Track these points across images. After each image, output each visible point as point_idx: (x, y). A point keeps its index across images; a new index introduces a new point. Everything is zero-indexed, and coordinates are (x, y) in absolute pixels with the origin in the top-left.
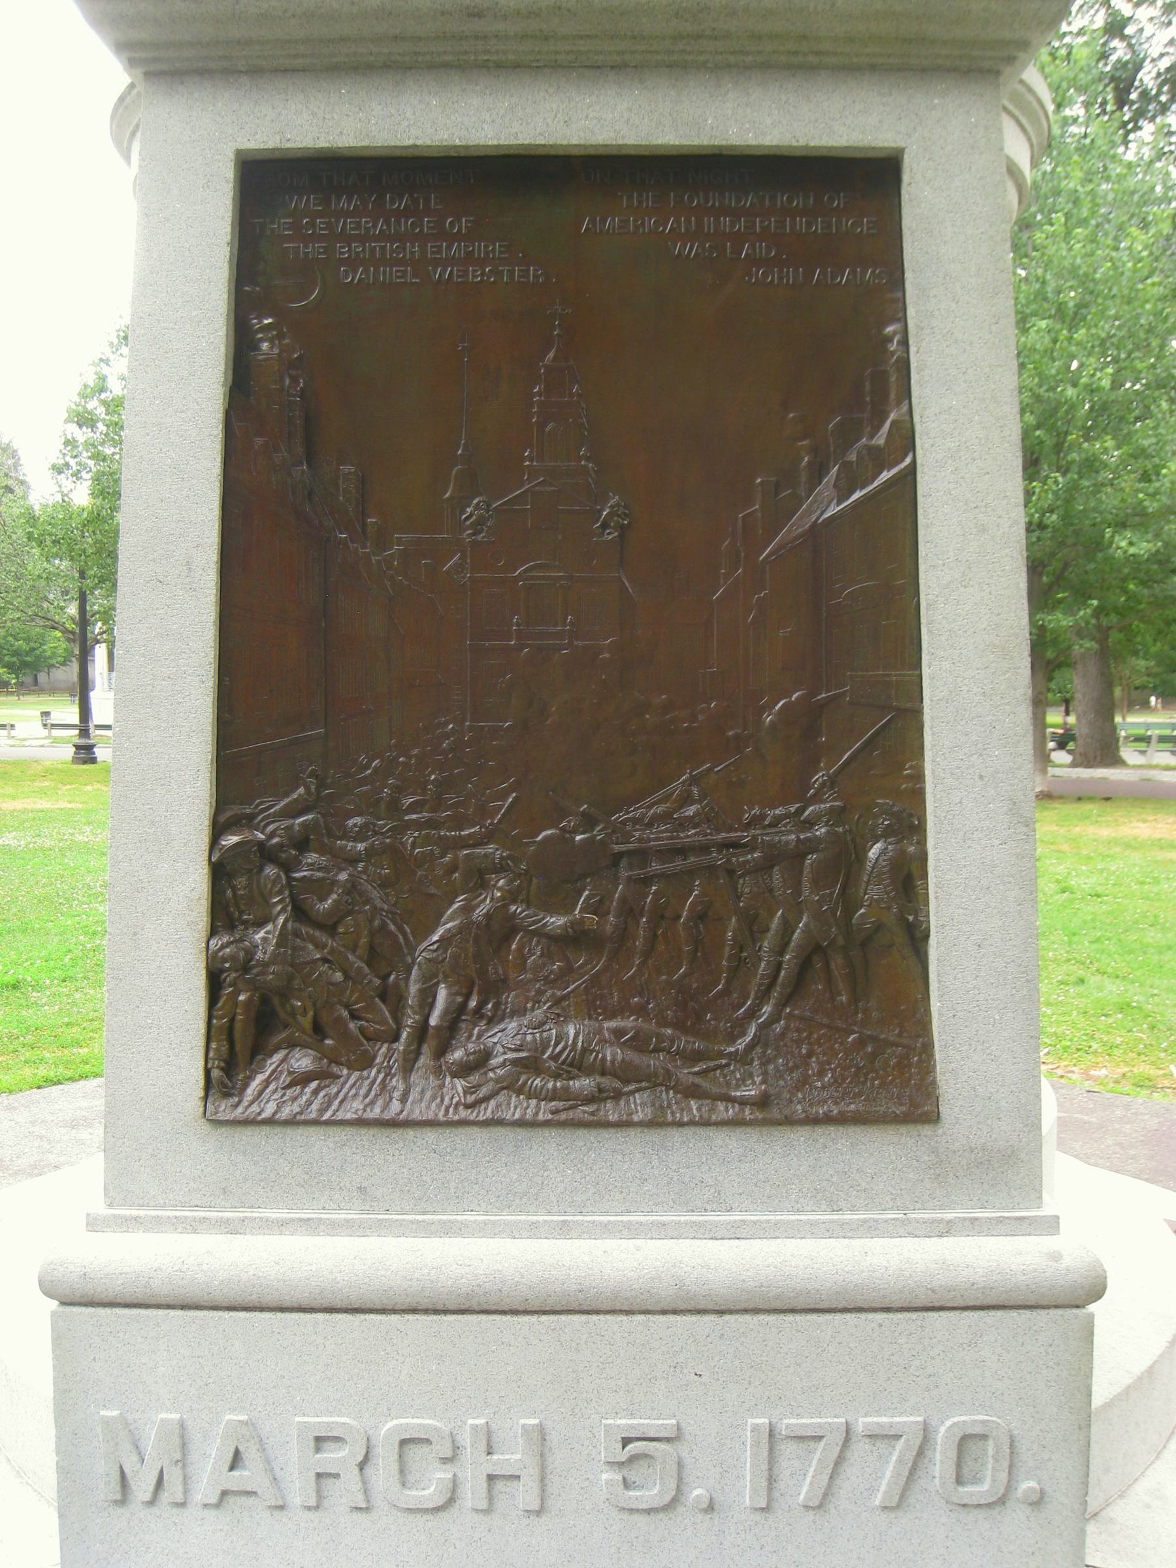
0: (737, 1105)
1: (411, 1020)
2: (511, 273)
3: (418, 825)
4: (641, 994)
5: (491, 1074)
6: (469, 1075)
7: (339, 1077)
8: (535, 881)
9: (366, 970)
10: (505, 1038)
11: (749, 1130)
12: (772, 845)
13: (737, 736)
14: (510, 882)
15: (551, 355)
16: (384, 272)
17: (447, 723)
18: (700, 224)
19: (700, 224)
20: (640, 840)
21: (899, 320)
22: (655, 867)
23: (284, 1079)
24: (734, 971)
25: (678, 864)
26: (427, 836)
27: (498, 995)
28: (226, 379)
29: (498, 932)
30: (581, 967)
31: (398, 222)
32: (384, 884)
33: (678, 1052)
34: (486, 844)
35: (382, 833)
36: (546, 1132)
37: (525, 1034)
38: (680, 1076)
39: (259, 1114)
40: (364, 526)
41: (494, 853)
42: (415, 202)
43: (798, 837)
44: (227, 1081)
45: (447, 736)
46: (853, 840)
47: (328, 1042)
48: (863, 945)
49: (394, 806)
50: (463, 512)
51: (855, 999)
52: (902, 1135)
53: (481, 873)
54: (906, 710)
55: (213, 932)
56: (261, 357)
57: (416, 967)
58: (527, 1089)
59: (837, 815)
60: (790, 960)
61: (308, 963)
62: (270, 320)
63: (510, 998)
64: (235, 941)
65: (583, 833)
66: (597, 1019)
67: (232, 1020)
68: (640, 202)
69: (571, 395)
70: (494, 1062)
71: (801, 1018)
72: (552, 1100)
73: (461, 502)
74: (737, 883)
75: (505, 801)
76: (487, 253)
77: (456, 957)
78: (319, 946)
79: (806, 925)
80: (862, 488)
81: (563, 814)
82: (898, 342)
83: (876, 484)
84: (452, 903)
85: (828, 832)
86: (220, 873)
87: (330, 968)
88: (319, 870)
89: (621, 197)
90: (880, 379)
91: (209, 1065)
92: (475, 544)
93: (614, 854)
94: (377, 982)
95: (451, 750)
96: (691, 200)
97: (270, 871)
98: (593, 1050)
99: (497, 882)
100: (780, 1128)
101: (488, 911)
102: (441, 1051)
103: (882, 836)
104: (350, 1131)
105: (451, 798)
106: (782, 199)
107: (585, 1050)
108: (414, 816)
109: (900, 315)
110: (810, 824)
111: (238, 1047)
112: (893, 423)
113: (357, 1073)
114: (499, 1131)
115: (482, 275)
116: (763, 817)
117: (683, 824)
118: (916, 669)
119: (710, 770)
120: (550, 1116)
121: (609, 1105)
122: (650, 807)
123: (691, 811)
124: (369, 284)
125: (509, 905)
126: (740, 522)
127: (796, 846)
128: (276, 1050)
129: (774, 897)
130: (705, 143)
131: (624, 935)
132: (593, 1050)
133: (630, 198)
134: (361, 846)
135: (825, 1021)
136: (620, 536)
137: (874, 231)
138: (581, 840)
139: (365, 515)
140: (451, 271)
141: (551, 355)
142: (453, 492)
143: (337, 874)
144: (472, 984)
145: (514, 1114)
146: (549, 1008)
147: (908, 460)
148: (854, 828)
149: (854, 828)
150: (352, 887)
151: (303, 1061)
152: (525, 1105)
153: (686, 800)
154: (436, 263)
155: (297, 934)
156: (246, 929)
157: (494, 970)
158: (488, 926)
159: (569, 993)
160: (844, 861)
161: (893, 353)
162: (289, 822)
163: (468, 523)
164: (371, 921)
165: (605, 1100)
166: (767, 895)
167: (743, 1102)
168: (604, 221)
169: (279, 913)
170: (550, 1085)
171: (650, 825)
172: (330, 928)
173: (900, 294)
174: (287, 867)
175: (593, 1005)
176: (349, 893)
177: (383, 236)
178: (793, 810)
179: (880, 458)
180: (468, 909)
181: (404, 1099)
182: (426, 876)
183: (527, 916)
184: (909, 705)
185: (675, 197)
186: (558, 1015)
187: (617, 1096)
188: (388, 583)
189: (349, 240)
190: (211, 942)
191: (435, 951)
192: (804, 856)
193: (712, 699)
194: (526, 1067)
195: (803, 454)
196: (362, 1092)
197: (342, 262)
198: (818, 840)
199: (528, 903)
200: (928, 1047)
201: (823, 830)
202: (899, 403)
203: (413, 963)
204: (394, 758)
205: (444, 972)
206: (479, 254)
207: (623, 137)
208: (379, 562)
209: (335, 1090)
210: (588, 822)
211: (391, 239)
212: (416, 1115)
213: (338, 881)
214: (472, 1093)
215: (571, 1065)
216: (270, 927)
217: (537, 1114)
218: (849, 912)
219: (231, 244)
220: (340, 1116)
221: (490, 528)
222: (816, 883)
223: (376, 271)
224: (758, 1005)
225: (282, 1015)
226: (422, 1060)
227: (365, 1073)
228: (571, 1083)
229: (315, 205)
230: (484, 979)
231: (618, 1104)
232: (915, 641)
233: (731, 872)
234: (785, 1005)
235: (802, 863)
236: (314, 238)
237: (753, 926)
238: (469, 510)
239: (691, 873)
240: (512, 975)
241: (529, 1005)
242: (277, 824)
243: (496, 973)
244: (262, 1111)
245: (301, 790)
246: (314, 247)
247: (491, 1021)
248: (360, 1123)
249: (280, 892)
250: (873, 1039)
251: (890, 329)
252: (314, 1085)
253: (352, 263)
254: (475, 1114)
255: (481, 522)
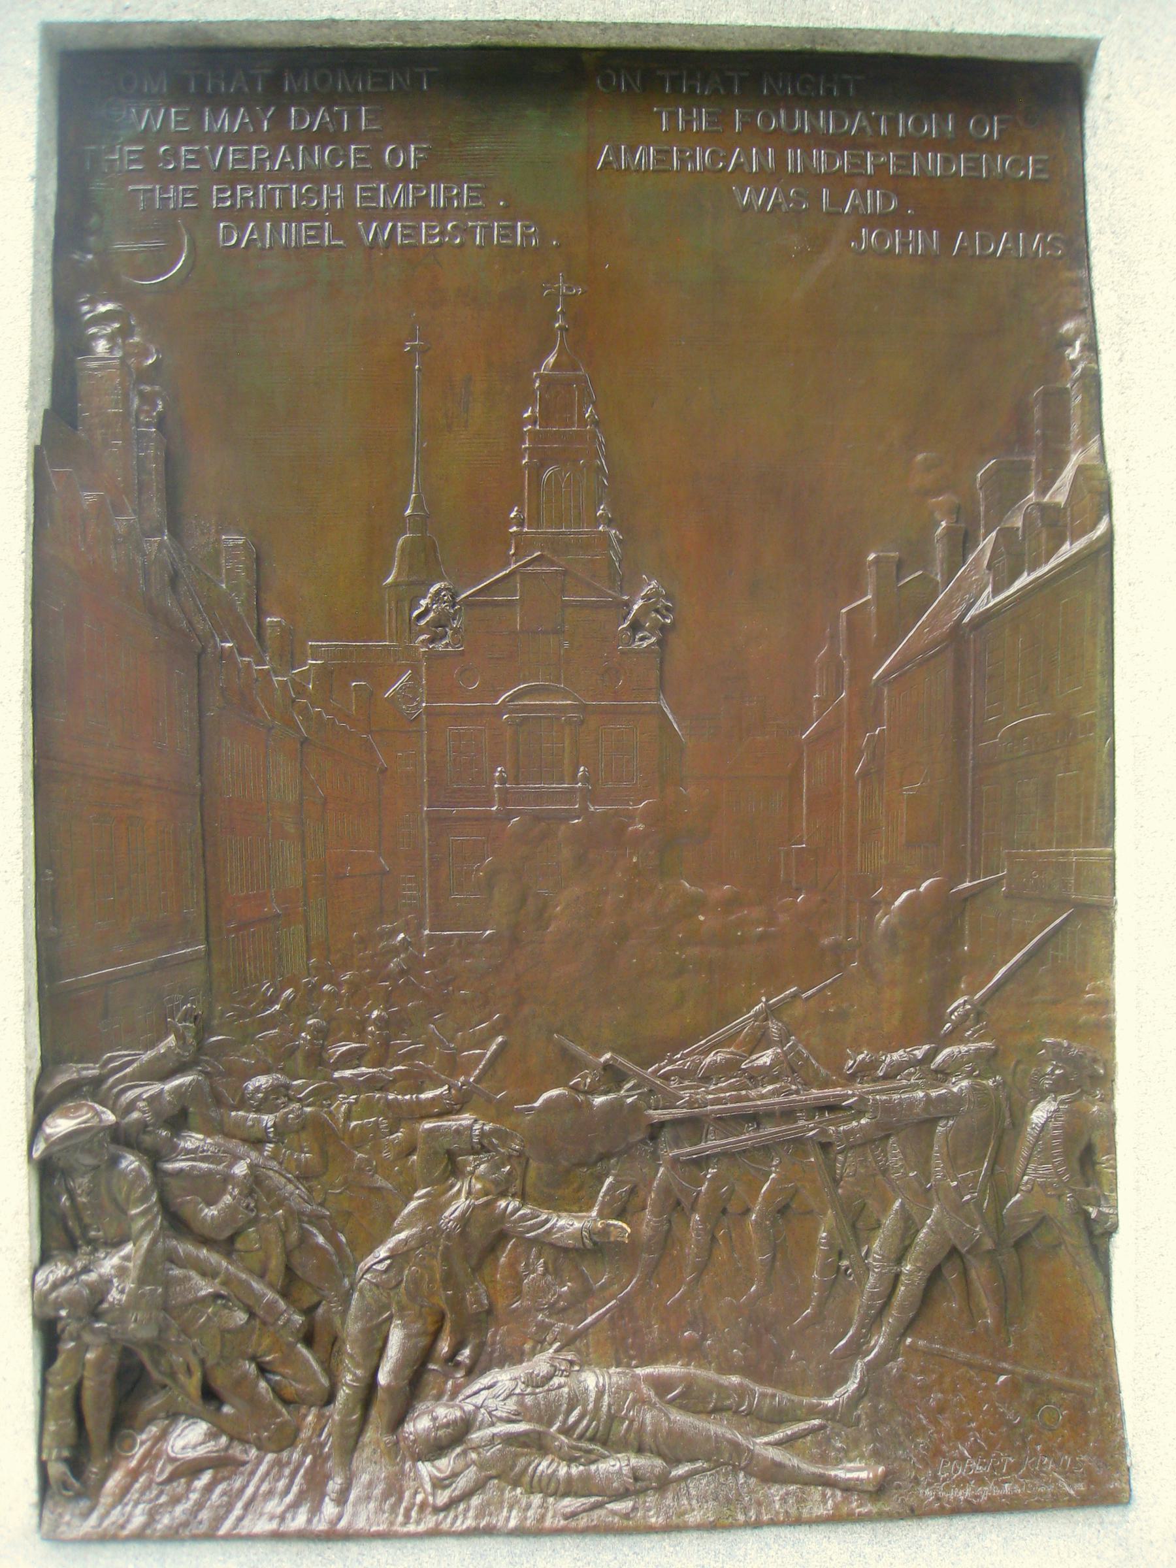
0: (839, 1493)
1: (350, 1378)
2: (488, 230)
3: (353, 1085)
4: (692, 1325)
5: (474, 1456)
6: (439, 1457)
7: (244, 1463)
8: (533, 1164)
9: (282, 1304)
10: (496, 1393)
11: (858, 1528)
12: (888, 1108)
13: (836, 948)
14: (496, 1167)
15: (551, 360)
16: (288, 231)
17: (394, 933)
18: (781, 160)
19: (781, 160)
20: (691, 1104)
21: (1083, 312)
22: (712, 1143)
23: (163, 1470)
24: (829, 1288)
25: (747, 1136)
26: (369, 1100)
27: (481, 1330)
28: (33, 398)
29: (485, 1240)
30: (603, 1287)
31: (309, 152)
32: (305, 1176)
33: (749, 1413)
34: (458, 1112)
35: (300, 1100)
36: (558, 1542)
37: (522, 1395)
38: (758, 1449)
39: (123, 1527)
40: (260, 627)
41: (470, 1127)
42: (337, 119)
43: (927, 1095)
44: (72, 1480)
45: (396, 951)
46: (1008, 1098)
47: (227, 1409)
48: (1018, 1245)
49: (317, 1059)
50: (414, 605)
51: (1005, 1319)
52: (1077, 1523)
53: (451, 1155)
54: (1091, 906)
55: (45, 1257)
56: (94, 364)
57: (356, 1295)
58: (527, 1479)
59: (987, 1062)
60: (911, 1272)
61: (191, 1303)
62: (110, 306)
63: (497, 1335)
64: (77, 1275)
65: (606, 1093)
66: (629, 1366)
67: (78, 1389)
68: (688, 123)
69: (582, 421)
70: (475, 1436)
71: (928, 1353)
72: (566, 1495)
73: (414, 588)
74: (835, 1160)
75: (486, 1048)
76: (449, 199)
77: (416, 1281)
78: (208, 1273)
79: (937, 1223)
80: (1032, 569)
81: (573, 1064)
82: (1083, 345)
83: (1053, 563)
84: (409, 1199)
85: (972, 1088)
86: (49, 1171)
87: (225, 1306)
88: (204, 1159)
89: (660, 114)
90: (1057, 400)
91: (44, 1457)
92: (432, 656)
93: (652, 1125)
94: (298, 1319)
95: (402, 973)
96: (767, 119)
97: (130, 1162)
98: (626, 1417)
99: (475, 1168)
100: (902, 1523)
101: (463, 1213)
102: (397, 1422)
103: (1049, 1091)
104: (261, 1548)
105: (404, 1044)
106: (905, 124)
107: (612, 1418)
108: (348, 1073)
109: (1085, 304)
110: (943, 1074)
111: (90, 1424)
112: (1081, 470)
113: (270, 1457)
114: (486, 1543)
115: (442, 233)
116: (873, 1065)
117: (757, 1077)
118: (1106, 846)
119: (795, 996)
120: (562, 1522)
121: (651, 1499)
122: (706, 1053)
123: (765, 1058)
124: (263, 249)
125: (496, 1200)
126: (843, 623)
127: (925, 1109)
128: (150, 1421)
129: (890, 1181)
130: (794, 24)
131: (666, 1240)
132: (626, 1417)
133: (673, 116)
134: (268, 1120)
135: (963, 1356)
136: (660, 642)
137: (1044, 176)
138: (603, 1104)
139: (261, 612)
140: (394, 228)
141: (551, 360)
142: (399, 574)
143: (231, 1166)
144: (442, 1318)
145: (508, 1519)
146: (556, 1351)
147: (1102, 528)
148: (1009, 1079)
149: (1009, 1079)
150: (256, 1178)
151: (190, 1438)
152: (524, 1502)
153: (760, 1041)
154: (370, 214)
155: (172, 1259)
156: (96, 1250)
157: (475, 1296)
158: (463, 1234)
159: (587, 1328)
160: (993, 1130)
161: (1073, 365)
162: (155, 1088)
163: (423, 623)
164: (284, 1233)
165: (643, 1491)
166: (880, 1177)
167: (848, 1488)
168: (632, 151)
169: (143, 1231)
170: (563, 1471)
171: (706, 1079)
172: (228, 1246)
173: (1084, 273)
174: (154, 1157)
175: (624, 1343)
176: (251, 1193)
177: (286, 175)
178: (919, 1054)
179: (1057, 526)
180: (433, 1208)
181: (342, 1499)
182: (369, 1161)
183: (524, 1218)
184: (1095, 898)
185: (743, 115)
186: (572, 1363)
187: (663, 1484)
188: (298, 719)
189: (232, 179)
190: (39, 1278)
191: (386, 1271)
192: (934, 1121)
193: (798, 891)
194: (525, 1445)
195: (937, 516)
196: (281, 1484)
197: (220, 214)
198: (958, 1098)
199: (524, 1197)
200: (1111, 1393)
201: (965, 1083)
202: (1084, 441)
203: (353, 1287)
204: (314, 986)
205: (398, 1303)
206: (437, 200)
207: (665, 12)
208: (284, 685)
209: (238, 1484)
210: (613, 1077)
211: (299, 178)
212: (361, 1524)
213: (233, 1176)
214: (445, 1487)
215: (592, 1440)
216: (128, 1248)
217: (543, 1517)
218: (1000, 1200)
219: (39, 178)
220: (244, 1528)
221: (456, 631)
222: (953, 1161)
223: (276, 229)
224: (865, 1336)
225: (155, 1375)
226: (369, 1435)
227: (285, 1455)
228: (593, 1468)
229: (177, 123)
230: (461, 1323)
231: (663, 1497)
232: (1107, 803)
233: (826, 1147)
234: (903, 1336)
235: (932, 1132)
236: (175, 176)
237: (857, 1223)
238: (423, 602)
239: (766, 1149)
240: (501, 1303)
241: (527, 1347)
242: (137, 1091)
243: (478, 1301)
244: (128, 1521)
245: (171, 1040)
246: (176, 190)
247: (473, 1371)
248: (277, 1536)
249: (144, 1198)
250: (1032, 1380)
251: (1068, 327)
252: (206, 1477)
253: (238, 216)
254: (449, 1520)
255: (441, 623)
